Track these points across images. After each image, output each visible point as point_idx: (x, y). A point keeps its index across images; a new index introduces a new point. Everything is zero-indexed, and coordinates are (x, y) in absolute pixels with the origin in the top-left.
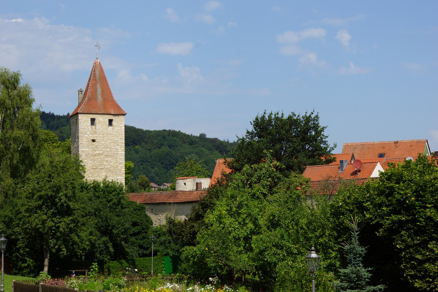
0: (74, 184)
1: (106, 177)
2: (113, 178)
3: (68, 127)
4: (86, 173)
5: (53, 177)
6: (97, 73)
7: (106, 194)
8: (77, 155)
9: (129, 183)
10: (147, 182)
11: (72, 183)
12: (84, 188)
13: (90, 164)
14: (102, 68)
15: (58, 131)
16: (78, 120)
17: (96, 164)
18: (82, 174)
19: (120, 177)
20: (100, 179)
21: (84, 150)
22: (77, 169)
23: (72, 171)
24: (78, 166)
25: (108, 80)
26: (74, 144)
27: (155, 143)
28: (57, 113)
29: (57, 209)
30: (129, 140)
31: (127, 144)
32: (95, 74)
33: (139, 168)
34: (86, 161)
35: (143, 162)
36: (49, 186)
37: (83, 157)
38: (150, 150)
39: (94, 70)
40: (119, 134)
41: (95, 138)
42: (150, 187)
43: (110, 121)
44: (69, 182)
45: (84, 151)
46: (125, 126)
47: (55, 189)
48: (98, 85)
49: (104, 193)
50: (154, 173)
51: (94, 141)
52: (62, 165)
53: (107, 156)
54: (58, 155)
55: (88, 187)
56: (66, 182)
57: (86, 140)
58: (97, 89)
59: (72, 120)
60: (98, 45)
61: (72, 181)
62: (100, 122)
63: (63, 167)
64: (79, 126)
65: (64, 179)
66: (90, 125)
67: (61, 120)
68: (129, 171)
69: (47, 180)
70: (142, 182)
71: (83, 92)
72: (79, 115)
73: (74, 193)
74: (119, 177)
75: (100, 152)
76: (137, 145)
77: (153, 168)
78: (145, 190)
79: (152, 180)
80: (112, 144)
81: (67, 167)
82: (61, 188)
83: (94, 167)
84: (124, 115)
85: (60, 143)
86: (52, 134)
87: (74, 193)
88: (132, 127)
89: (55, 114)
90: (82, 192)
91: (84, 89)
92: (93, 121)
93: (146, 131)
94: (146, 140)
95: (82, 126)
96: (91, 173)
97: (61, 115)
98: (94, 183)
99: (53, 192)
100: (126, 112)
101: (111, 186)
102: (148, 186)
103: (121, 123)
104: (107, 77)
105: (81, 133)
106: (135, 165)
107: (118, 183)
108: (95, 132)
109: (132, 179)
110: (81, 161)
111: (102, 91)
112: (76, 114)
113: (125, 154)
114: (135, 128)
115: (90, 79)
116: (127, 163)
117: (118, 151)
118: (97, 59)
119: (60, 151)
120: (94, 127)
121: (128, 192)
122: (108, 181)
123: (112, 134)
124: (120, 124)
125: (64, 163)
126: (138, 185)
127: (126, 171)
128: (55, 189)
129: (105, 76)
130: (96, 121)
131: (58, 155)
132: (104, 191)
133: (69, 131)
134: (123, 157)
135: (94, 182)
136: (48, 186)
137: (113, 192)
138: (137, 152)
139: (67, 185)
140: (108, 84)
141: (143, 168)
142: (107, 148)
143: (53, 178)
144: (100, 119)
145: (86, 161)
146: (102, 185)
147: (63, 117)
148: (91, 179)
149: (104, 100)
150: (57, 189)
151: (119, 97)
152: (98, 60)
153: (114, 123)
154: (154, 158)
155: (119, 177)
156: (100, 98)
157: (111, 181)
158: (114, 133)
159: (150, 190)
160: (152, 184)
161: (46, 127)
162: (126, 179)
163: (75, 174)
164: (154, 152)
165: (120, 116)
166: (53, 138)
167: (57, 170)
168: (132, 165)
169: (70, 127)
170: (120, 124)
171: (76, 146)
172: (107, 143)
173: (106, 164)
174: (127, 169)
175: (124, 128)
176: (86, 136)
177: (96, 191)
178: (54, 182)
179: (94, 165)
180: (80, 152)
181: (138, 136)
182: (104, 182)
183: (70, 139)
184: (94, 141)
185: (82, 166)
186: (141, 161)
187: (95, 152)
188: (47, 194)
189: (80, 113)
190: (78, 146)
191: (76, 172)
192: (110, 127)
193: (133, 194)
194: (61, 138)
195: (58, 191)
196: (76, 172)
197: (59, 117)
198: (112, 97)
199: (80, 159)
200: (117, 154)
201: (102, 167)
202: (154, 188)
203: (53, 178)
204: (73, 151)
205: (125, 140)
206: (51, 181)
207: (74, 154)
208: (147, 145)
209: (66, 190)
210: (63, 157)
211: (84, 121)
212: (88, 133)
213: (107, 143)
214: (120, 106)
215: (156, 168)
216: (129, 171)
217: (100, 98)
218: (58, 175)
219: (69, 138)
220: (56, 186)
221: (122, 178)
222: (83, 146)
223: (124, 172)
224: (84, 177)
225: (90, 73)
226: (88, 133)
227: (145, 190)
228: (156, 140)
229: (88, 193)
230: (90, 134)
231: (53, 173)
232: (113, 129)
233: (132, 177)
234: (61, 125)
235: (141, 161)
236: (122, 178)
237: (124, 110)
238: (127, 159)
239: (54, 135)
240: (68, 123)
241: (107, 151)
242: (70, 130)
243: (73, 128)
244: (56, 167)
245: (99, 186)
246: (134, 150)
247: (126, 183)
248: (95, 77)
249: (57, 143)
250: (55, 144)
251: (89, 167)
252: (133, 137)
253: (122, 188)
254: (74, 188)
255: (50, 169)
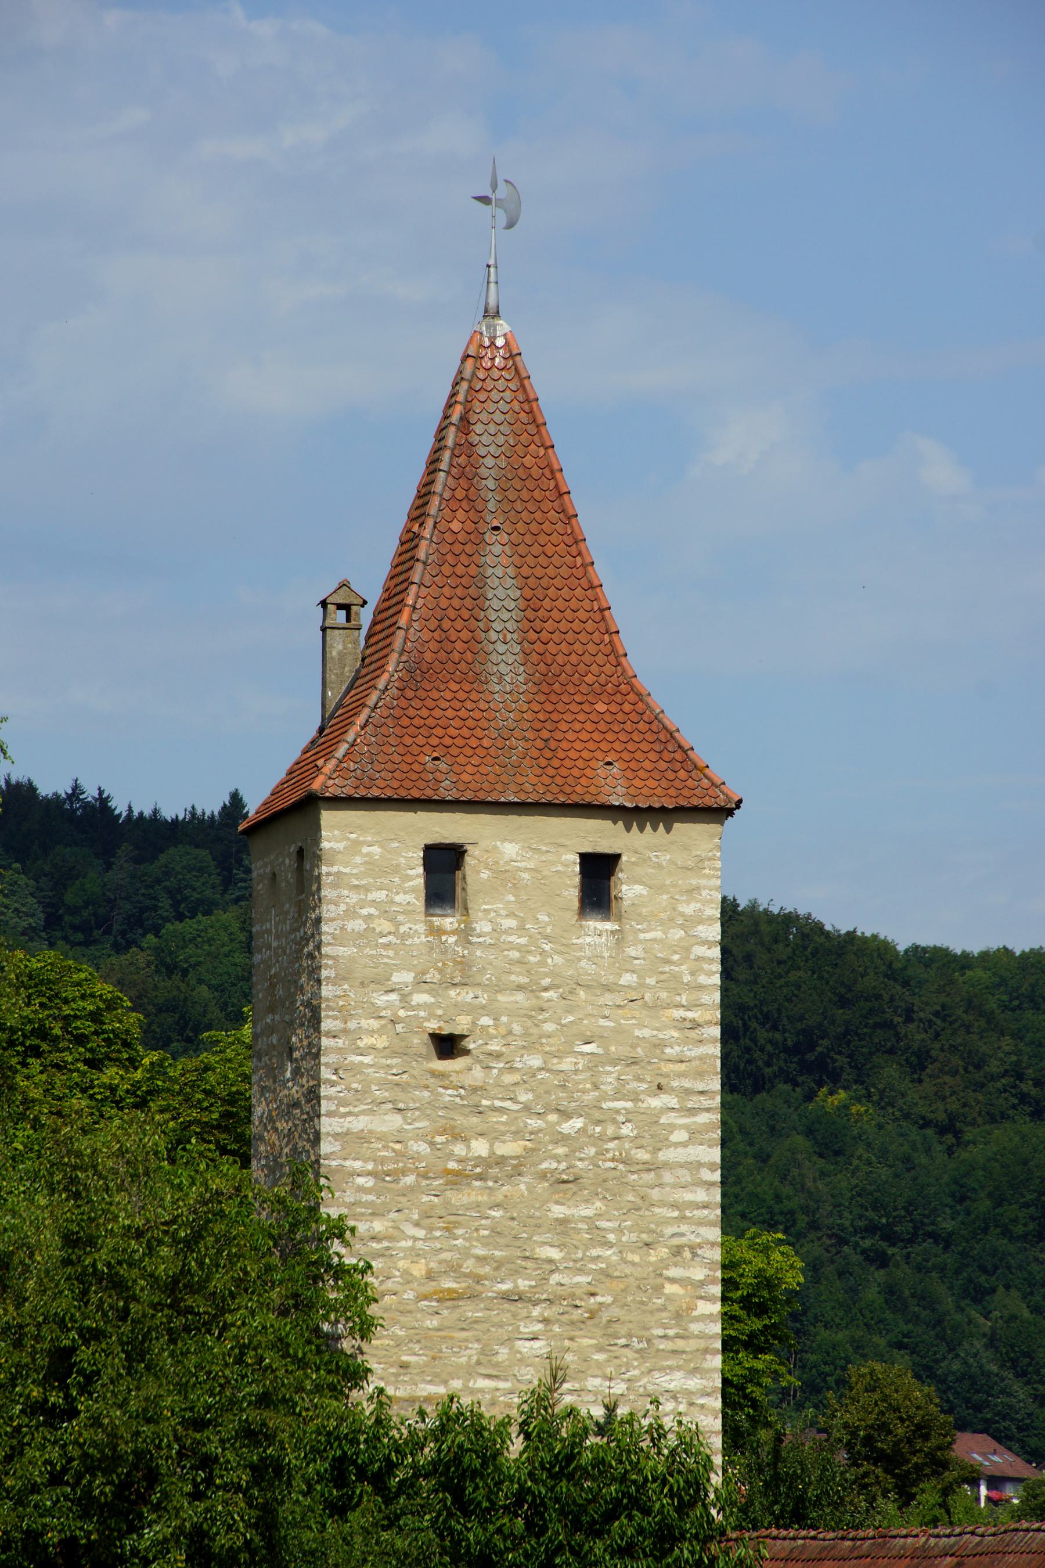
0: (270, 1438)
1: (557, 1376)
2: (619, 1388)
3: (228, 916)
4: (379, 1341)
5: (90, 1378)
6: (490, 439)
7: (557, 1530)
8: (304, 1172)
9: (764, 1435)
10: (922, 1430)
11: (251, 1435)
12: (362, 1473)
13: (415, 1255)
14: (529, 402)
15: (142, 958)
16: (317, 859)
17: (466, 1254)
18: (347, 1345)
19: (675, 1381)
20: (496, 1395)
21: (370, 1128)
22: (299, 1304)
23: (255, 1319)
24: (304, 1281)
25: (579, 502)
26: (274, 1073)
27: (994, 1067)
28: (133, 795)
29: (89, 1275)
30: (762, 1035)
31: (740, 1076)
32: (466, 448)
33: (853, 1291)
34: (378, 1226)
35: (891, 1238)
36: (55, 1454)
37: (350, 1189)
38: (949, 1127)
39: (458, 420)
40: (674, 984)
41: (461, 1025)
42: (949, 1476)
43: (598, 874)
44: (230, 1425)
45: (363, 1137)
46: (729, 911)
47: (101, 1487)
48: (497, 550)
49: (535, 1528)
50: (992, 1341)
51: (447, 1045)
52: (165, 1263)
53: (565, 1183)
54: (139, 1174)
55: (390, 1467)
56: (199, 1424)
57: (381, 1042)
58: (480, 581)
59: (265, 863)
60: (503, 191)
61: (253, 1415)
62: (505, 877)
63: (172, 1286)
64: (327, 911)
65: (183, 1389)
66: (420, 904)
67: (176, 856)
68: (757, 1324)
69: (34, 1408)
70: (884, 1428)
71: (366, 617)
72: (328, 818)
73: (267, 1521)
74: (668, 1379)
75: (501, 1149)
76: (835, 1079)
77: (978, 1295)
78: (906, 1498)
79: (975, 1411)
80: (609, 1078)
81: (219, 1282)
82: (153, 1477)
83: (449, 1284)
84: (721, 813)
85: (157, 1069)
86: (90, 983)
87: (267, 1521)
88: (789, 919)
89: (119, 806)
90: (339, 1509)
91: (371, 587)
92: (444, 865)
93: (916, 951)
94: (916, 1035)
95: (351, 913)
96: (419, 1337)
97: (168, 813)
98: (442, 1431)
99: (85, 1516)
100: (735, 789)
101: (599, 1463)
102: (939, 1464)
103: (692, 892)
104: (570, 479)
105: (335, 886)
106: (813, 1269)
107: (658, 1433)
108: (464, 964)
109: (785, 1392)
110: (339, 1230)
111: (530, 604)
112: (297, 811)
113: (728, 1166)
114: (819, 927)
115: (424, 494)
116: (742, 1251)
117: (661, 1143)
118: (491, 314)
119: (157, 1141)
120: (449, 922)
121: (747, 1518)
122: (571, 1412)
123: (607, 988)
124: (679, 896)
125: (189, 1244)
126: (842, 1456)
127: (728, 1318)
128: (101, 1487)
129: (553, 472)
130: (476, 872)
131: (139, 1174)
132: (538, 1507)
133: (239, 958)
134: (707, 1196)
135: (450, 1418)
136: (39, 1457)
137: (611, 1516)
138: (831, 1143)
139: (213, 1448)
140: (579, 540)
141: (890, 1291)
142: (566, 1115)
143: (85, 1389)
144: (510, 849)
145: (378, 1226)
146: (516, 1446)
147: (191, 830)
148: (426, 1389)
149: (549, 680)
150: (123, 1487)
151: (670, 649)
152: (502, 326)
153: (627, 888)
154: (983, 1205)
155: (668, 1379)
156: (506, 664)
157: (598, 1412)
158: (627, 979)
159: (957, 1503)
160: (976, 1451)
161: (38, 920)
162: (734, 1393)
163: (281, 1345)
164: (989, 1144)
165: (683, 830)
166: (95, 1017)
167: (124, 1315)
168: (788, 1267)
169: (246, 925)
170: (679, 896)
171: (295, 1092)
172: (567, 1064)
173: (554, 1254)
174: (745, 1302)
175: (715, 931)
176: (382, 1000)
177: (464, 1506)
178: (95, 1422)
179: (453, 1269)
180: (326, 1147)
181: (843, 1002)
182: (540, 1417)
183: (247, 1030)
184: (447, 1045)
185: (340, 1272)
186: (871, 1229)
187: (459, 1149)
188: (32, 1536)
189: (338, 802)
190: (313, 1096)
191: (285, 1325)
192: (594, 924)
193: (794, 1540)
194: (169, 1019)
195: (127, 1507)
196: (285, 1325)
197: (153, 833)
198: (616, 656)
199: (330, 1210)
200: (649, 1167)
201: (523, 1284)
202: (995, 1482)
203: (85, 1389)
204: (269, 1141)
205: (729, 1034)
206: (74, 1413)
207: (274, 1168)
208: (928, 1087)
209: (197, 1495)
210: (174, 1199)
211: (367, 861)
212: (403, 977)
213: (567, 1064)
214: (688, 736)
215: (1010, 1302)
216: (757, 1324)
217: (506, 664)
218: (136, 1354)
219: (239, 1019)
220: (117, 1459)
221: (694, 1383)
222: (360, 1095)
223: (716, 1328)
224: (357, 1375)
225: (429, 442)
226: (403, 977)
227: (906, 1498)
228: (1007, 1043)
229: (392, 1522)
230: (421, 983)
231: (91, 1336)
232: (620, 938)
233: (791, 1380)
234: (165, 902)
235: (871, 1229)
236: (694, 1383)
237: (718, 771)
238: (740, 1210)
239: (105, 989)
240: (228, 882)
241: (563, 1139)
242: (248, 948)
243: (270, 928)
244: (118, 1285)
245: (491, 1456)
246: (810, 1133)
247: (734, 1437)
248: (467, 474)
249: (133, 1063)
250: (111, 1074)
251: (408, 1278)
252: (801, 1012)
253: (697, 1485)
254: (269, 1473)
255: (64, 1304)
